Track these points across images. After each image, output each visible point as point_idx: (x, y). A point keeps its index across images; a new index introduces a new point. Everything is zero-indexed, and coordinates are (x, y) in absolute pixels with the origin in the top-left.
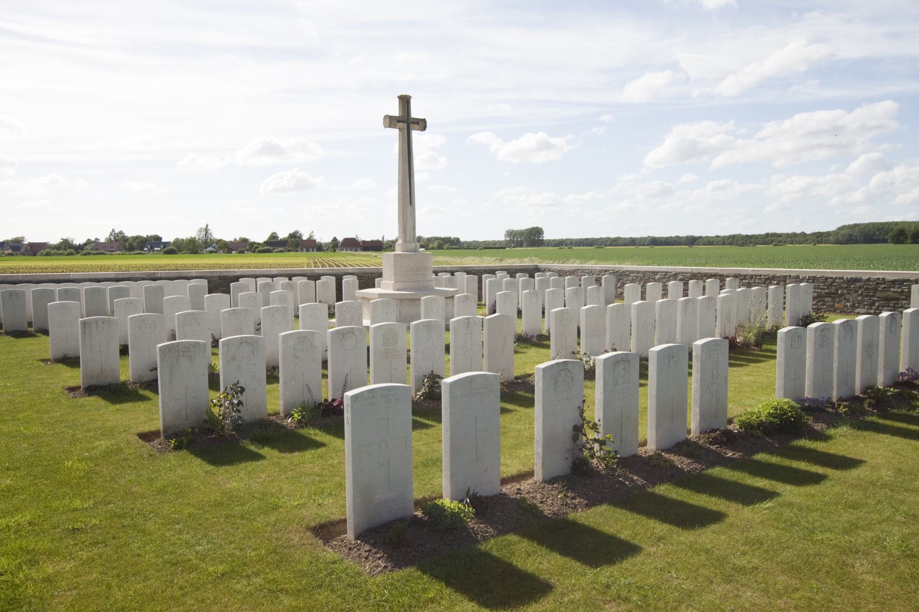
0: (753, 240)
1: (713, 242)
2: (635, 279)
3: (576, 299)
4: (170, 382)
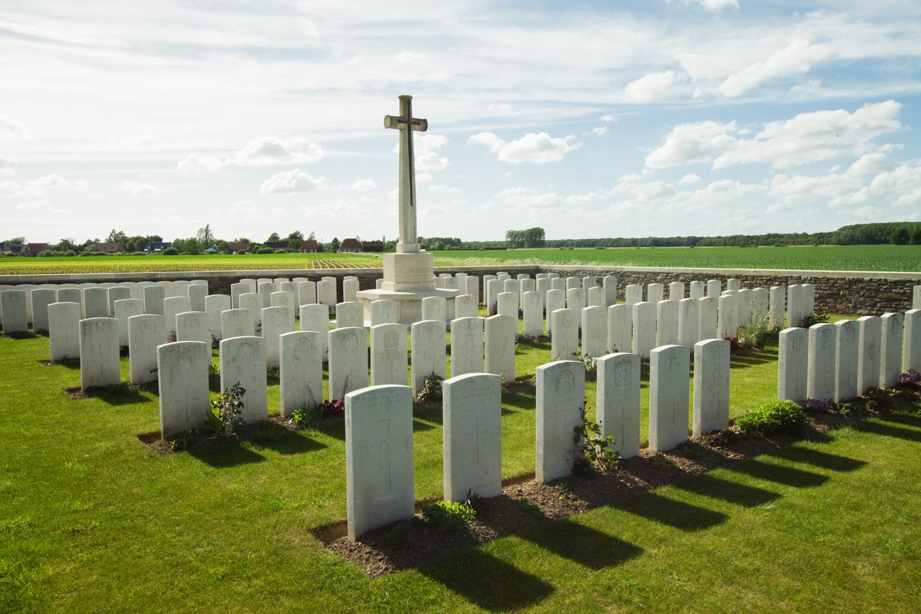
0: (754, 241)
1: (715, 242)
4: (170, 383)
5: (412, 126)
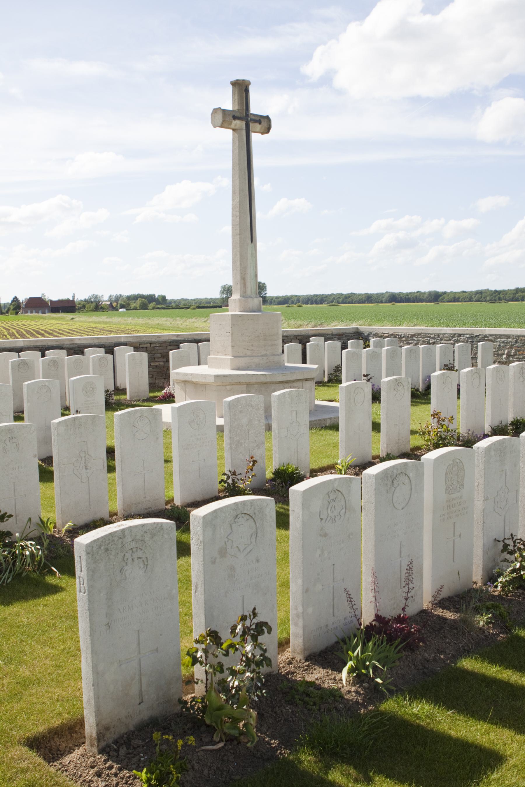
0: (501, 296)
1: (459, 298)
2: (503, 346)
3: (521, 379)
4: (108, 625)
5: (251, 125)
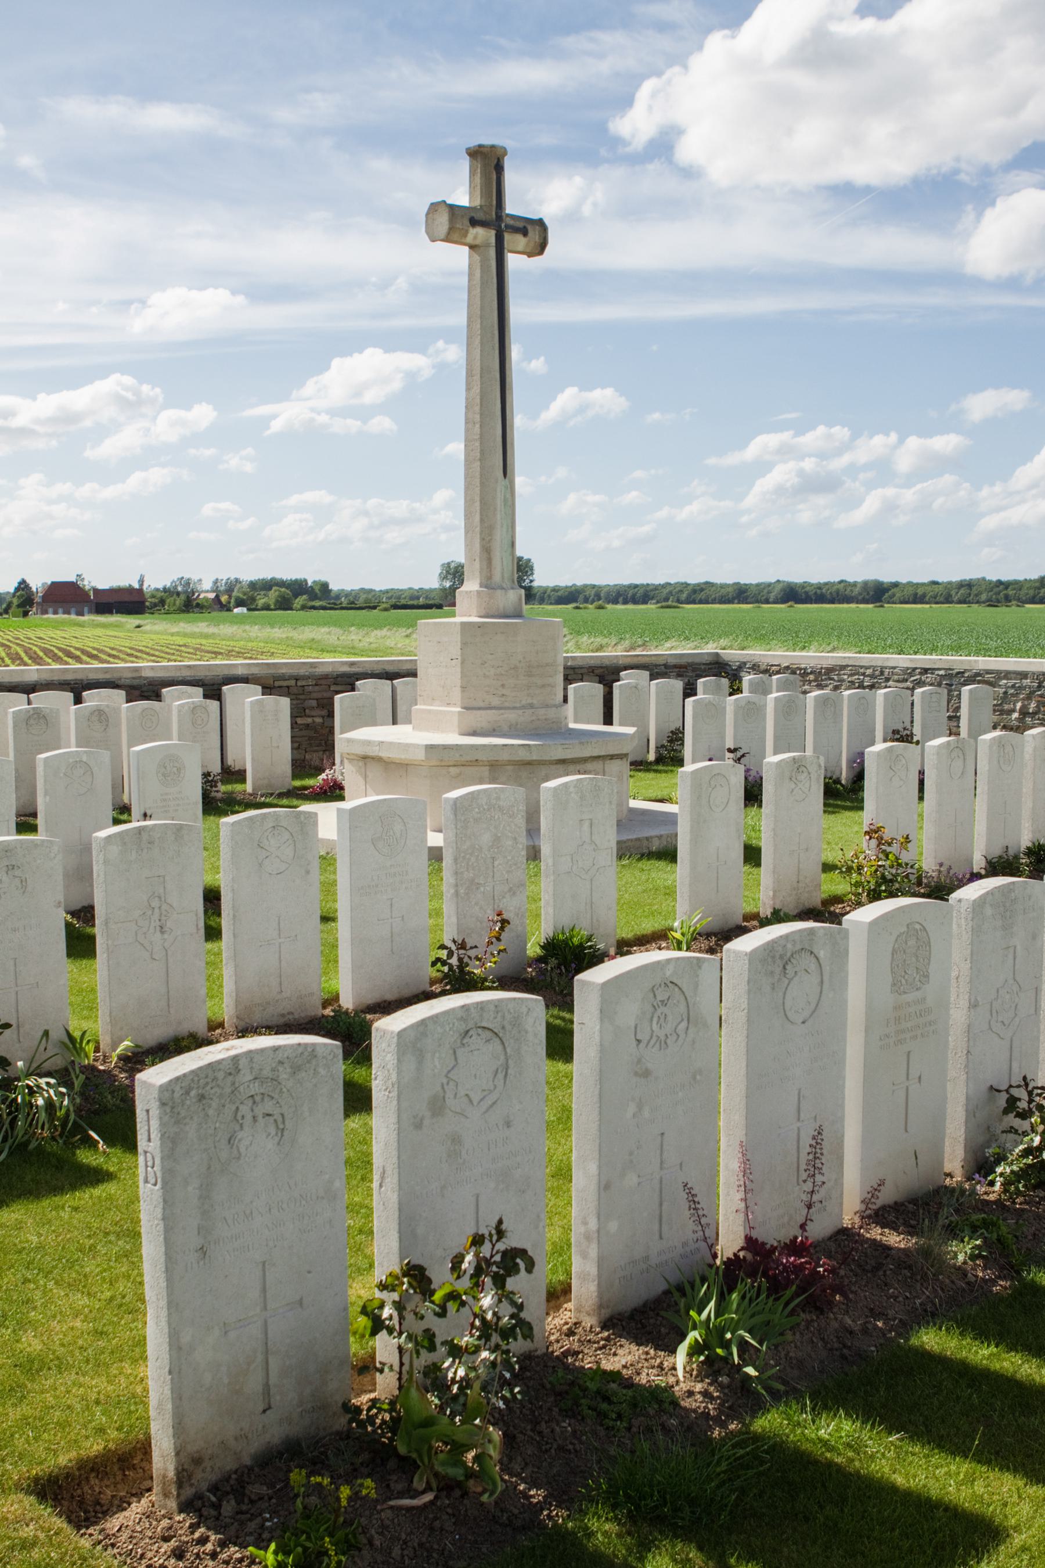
0: (1011, 592)
1: (924, 595)
4: (202, 1250)
5: (507, 237)
